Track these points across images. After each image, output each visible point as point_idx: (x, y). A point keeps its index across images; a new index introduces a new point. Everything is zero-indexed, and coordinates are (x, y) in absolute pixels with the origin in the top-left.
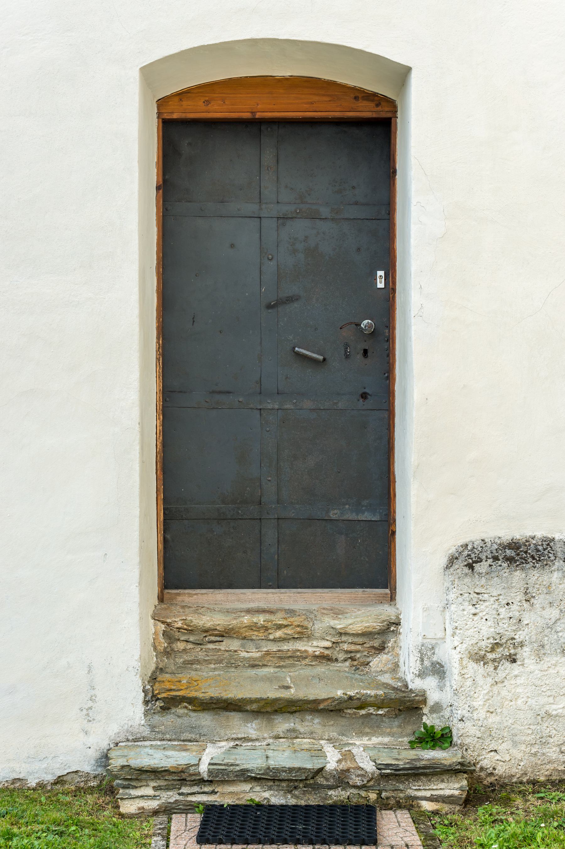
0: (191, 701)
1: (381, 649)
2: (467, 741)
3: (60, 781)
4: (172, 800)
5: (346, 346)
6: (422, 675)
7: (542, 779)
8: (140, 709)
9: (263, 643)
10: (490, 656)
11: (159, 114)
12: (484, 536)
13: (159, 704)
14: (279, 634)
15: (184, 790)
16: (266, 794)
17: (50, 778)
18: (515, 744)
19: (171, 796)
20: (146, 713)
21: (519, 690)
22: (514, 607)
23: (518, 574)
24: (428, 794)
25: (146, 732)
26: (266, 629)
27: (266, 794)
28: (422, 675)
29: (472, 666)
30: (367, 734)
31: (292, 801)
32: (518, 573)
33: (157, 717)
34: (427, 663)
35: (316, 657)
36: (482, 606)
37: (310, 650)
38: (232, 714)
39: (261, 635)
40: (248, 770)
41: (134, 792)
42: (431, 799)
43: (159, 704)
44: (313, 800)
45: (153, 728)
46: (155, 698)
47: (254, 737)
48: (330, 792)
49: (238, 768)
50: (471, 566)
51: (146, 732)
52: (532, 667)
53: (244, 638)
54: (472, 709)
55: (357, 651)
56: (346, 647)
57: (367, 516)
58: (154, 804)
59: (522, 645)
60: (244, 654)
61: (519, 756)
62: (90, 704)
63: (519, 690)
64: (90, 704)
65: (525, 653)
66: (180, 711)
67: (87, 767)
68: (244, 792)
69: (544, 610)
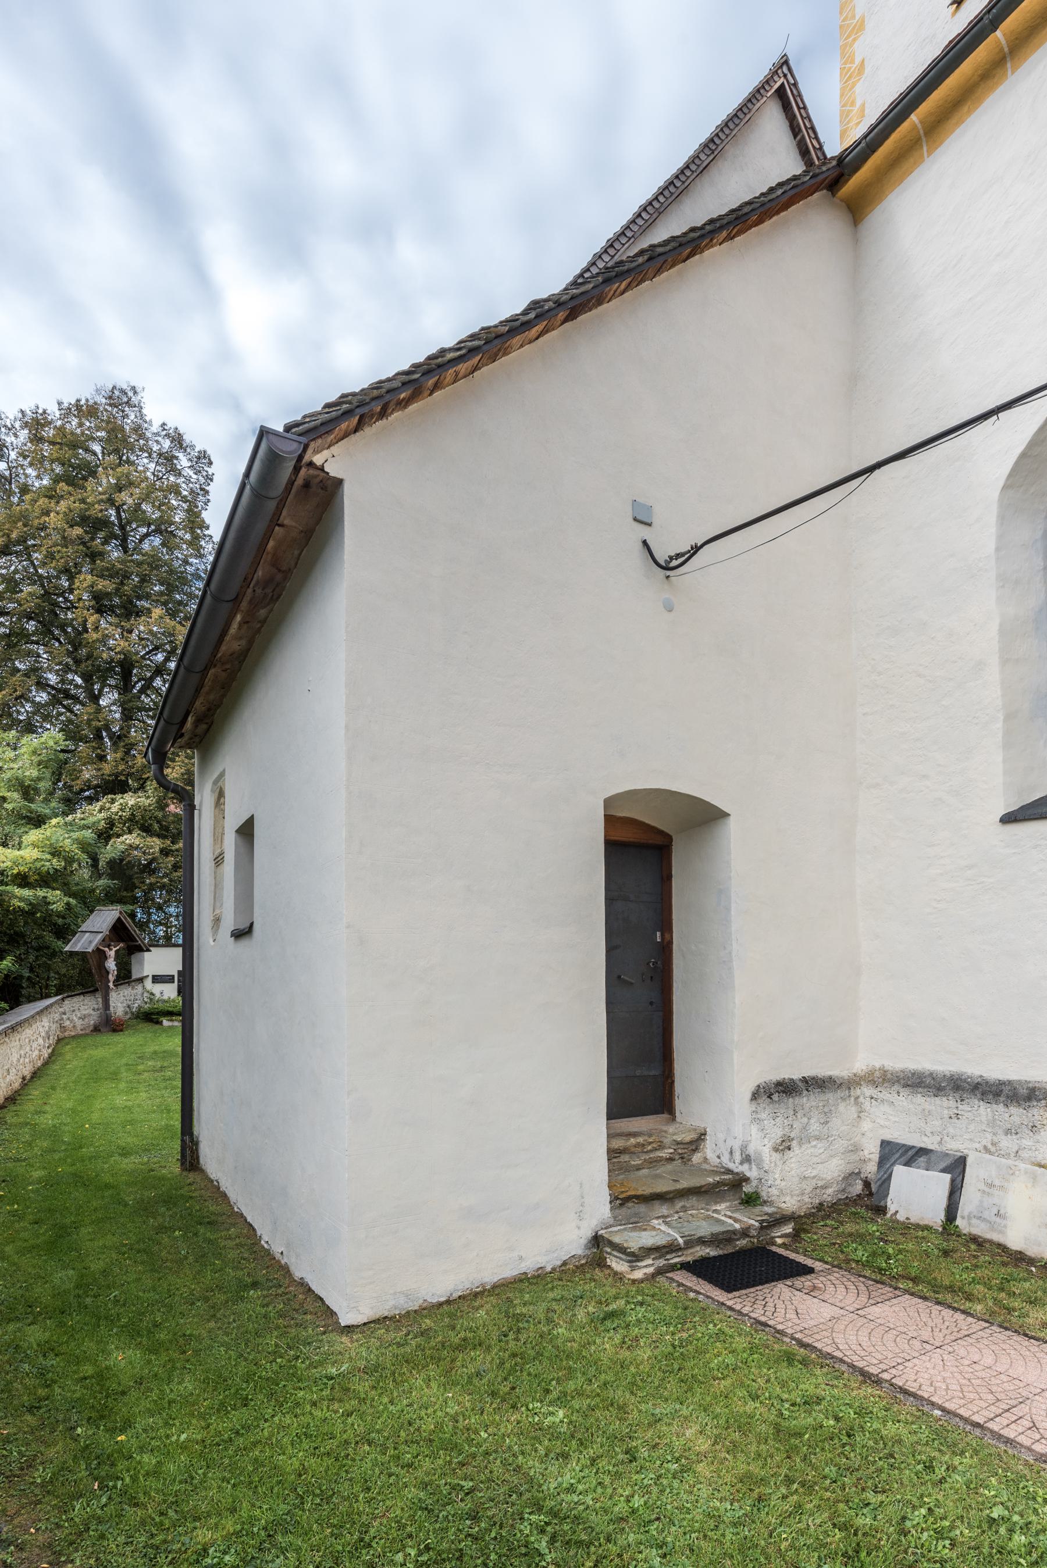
0: (637, 1197)
1: (695, 1151)
2: (773, 1198)
3: (565, 1263)
4: (661, 1265)
5: (643, 974)
6: (742, 1163)
7: (803, 1214)
8: (608, 1206)
9: (640, 1154)
10: (781, 1148)
11: (605, 836)
12: (765, 1080)
13: (618, 1202)
14: (650, 1148)
15: (668, 1257)
16: (707, 1251)
17: (559, 1263)
18: (792, 1196)
19: (661, 1262)
20: (612, 1209)
21: (793, 1165)
22: (790, 1119)
23: (791, 1100)
24: (779, 1234)
25: (611, 1221)
26: (643, 1145)
27: (707, 1251)
28: (742, 1163)
29: (774, 1154)
30: (718, 1203)
31: (721, 1252)
32: (791, 1099)
33: (617, 1211)
34: (744, 1156)
35: (667, 1159)
36: (777, 1120)
37: (664, 1155)
38: (655, 1202)
39: (639, 1150)
40: (702, 1237)
41: (639, 1264)
42: (779, 1237)
43: (618, 1202)
44: (729, 1250)
45: (615, 1218)
46: (617, 1198)
47: (666, 1214)
48: (738, 1243)
49: (696, 1237)
50: (769, 1097)
51: (611, 1221)
52: (797, 1152)
53: (632, 1153)
54: (775, 1179)
55: (685, 1153)
56: (680, 1151)
57: (653, 1073)
58: (651, 1270)
59: (793, 1139)
60: (633, 1163)
61: (794, 1203)
62: (581, 1208)
63: (793, 1165)
64: (581, 1208)
65: (794, 1144)
66: (630, 1204)
67: (580, 1252)
68: (697, 1251)
69: (958, 1119)
